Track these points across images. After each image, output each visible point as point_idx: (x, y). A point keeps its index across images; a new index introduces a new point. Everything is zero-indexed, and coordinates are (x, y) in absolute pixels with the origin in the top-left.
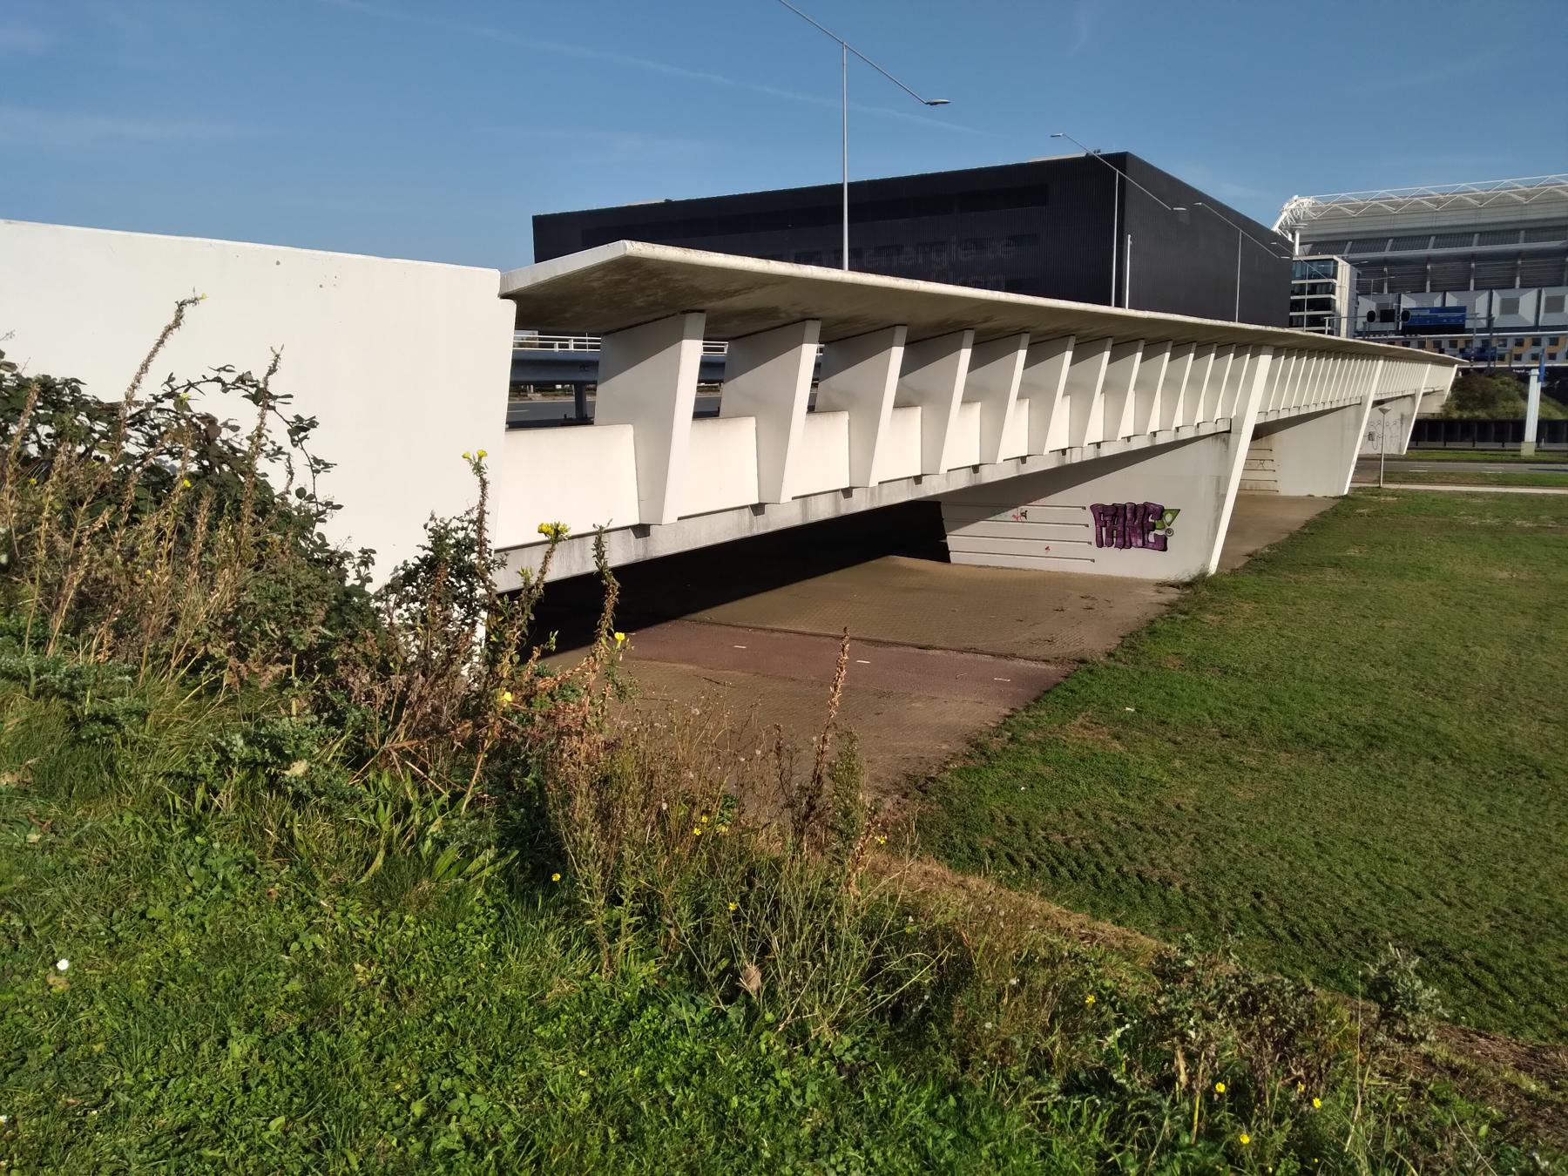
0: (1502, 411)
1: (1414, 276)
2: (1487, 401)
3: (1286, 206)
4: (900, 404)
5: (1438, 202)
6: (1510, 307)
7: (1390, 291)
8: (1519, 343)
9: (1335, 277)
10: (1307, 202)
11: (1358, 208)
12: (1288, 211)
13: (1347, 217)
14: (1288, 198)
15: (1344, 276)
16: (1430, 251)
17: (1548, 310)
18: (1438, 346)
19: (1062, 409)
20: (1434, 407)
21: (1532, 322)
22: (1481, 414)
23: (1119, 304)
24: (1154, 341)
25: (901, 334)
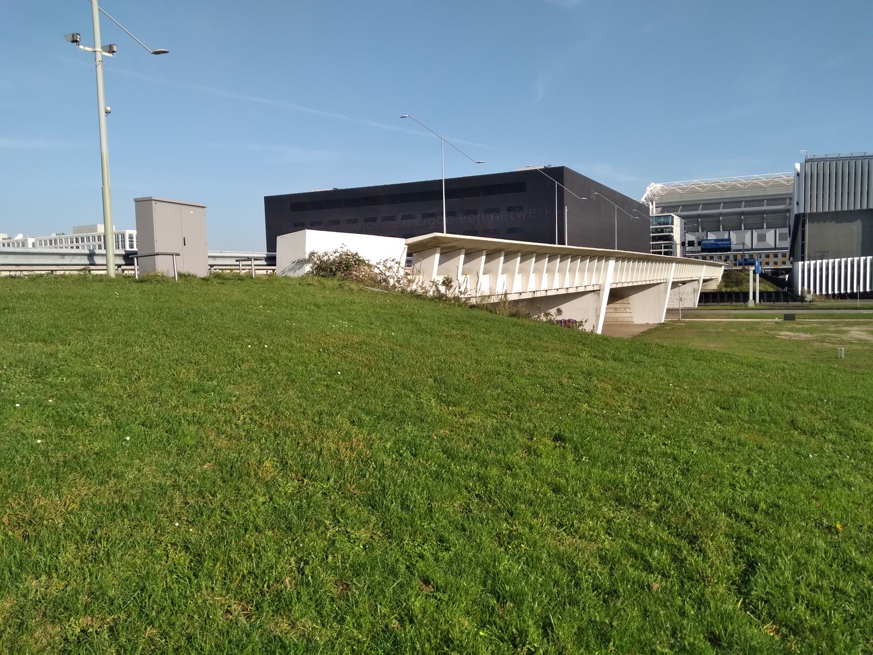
0: (743, 288)
1: (713, 223)
2: (738, 283)
3: (648, 188)
4: (484, 273)
5: (723, 186)
6: (762, 238)
7: (703, 231)
8: (768, 256)
9: (672, 224)
10: (659, 186)
11: (684, 189)
12: (648, 191)
13: (678, 193)
14: (648, 184)
15: (677, 225)
16: (721, 210)
17: (780, 240)
18: (704, 258)
19: (533, 277)
20: (713, 287)
21: (773, 246)
22: (736, 289)
23: (562, 242)
24: (574, 256)
25: (485, 252)
